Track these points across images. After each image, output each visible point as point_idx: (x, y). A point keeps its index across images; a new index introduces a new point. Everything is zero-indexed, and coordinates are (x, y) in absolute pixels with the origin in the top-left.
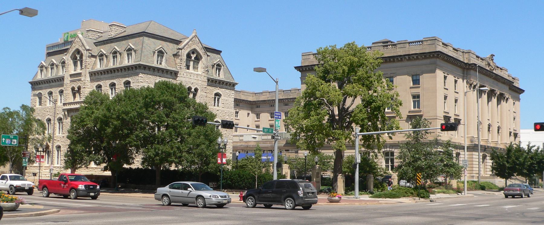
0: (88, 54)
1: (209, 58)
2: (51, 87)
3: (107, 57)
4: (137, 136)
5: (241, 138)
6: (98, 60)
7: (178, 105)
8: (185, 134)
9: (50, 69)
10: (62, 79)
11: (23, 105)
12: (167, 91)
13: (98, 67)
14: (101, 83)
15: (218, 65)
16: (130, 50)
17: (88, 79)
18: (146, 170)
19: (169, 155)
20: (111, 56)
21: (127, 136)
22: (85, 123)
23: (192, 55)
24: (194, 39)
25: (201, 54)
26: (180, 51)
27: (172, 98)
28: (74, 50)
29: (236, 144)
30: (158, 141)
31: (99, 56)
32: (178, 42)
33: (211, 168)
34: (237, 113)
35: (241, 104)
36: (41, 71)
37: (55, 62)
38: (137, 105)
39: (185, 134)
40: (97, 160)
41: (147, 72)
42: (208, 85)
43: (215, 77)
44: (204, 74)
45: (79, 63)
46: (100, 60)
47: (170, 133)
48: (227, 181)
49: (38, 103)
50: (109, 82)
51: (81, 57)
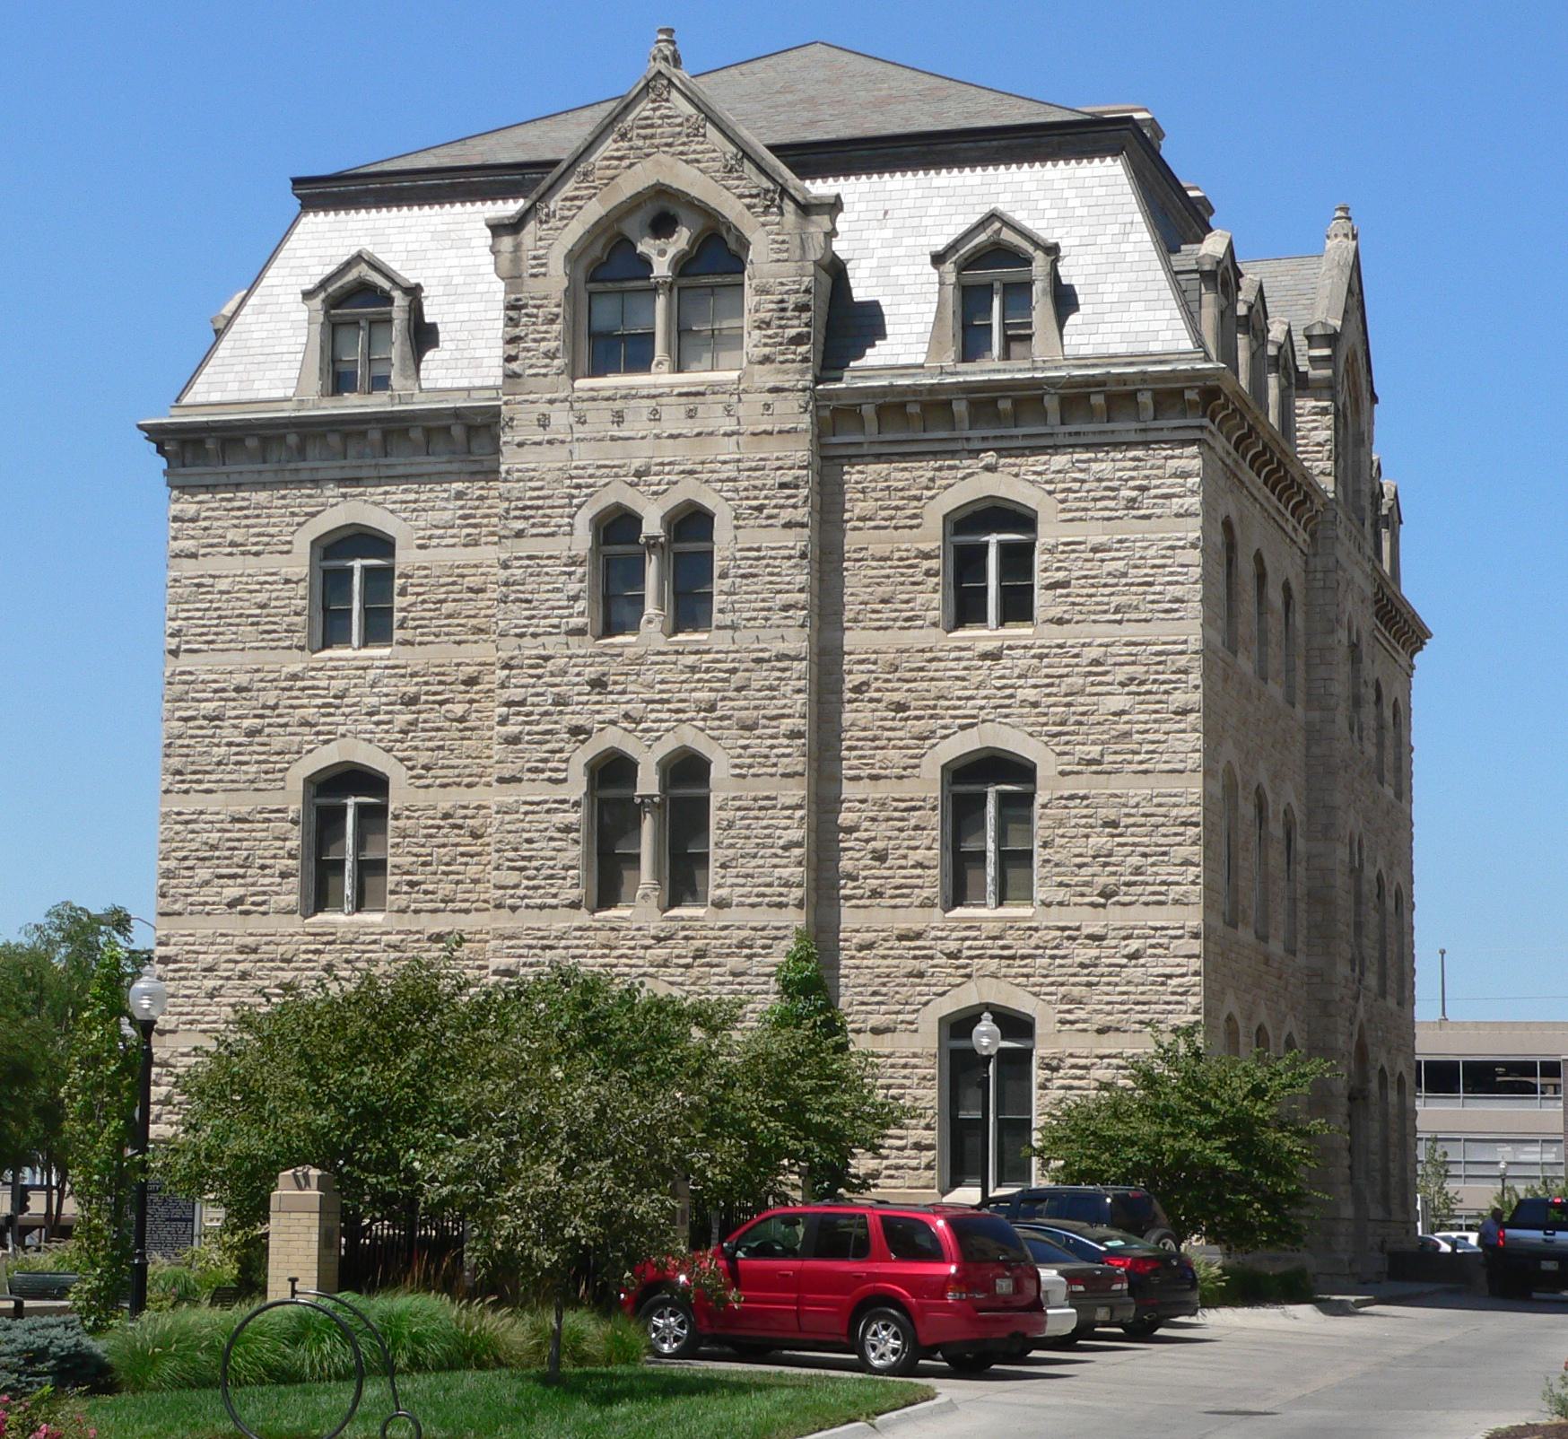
23: (646, 246)
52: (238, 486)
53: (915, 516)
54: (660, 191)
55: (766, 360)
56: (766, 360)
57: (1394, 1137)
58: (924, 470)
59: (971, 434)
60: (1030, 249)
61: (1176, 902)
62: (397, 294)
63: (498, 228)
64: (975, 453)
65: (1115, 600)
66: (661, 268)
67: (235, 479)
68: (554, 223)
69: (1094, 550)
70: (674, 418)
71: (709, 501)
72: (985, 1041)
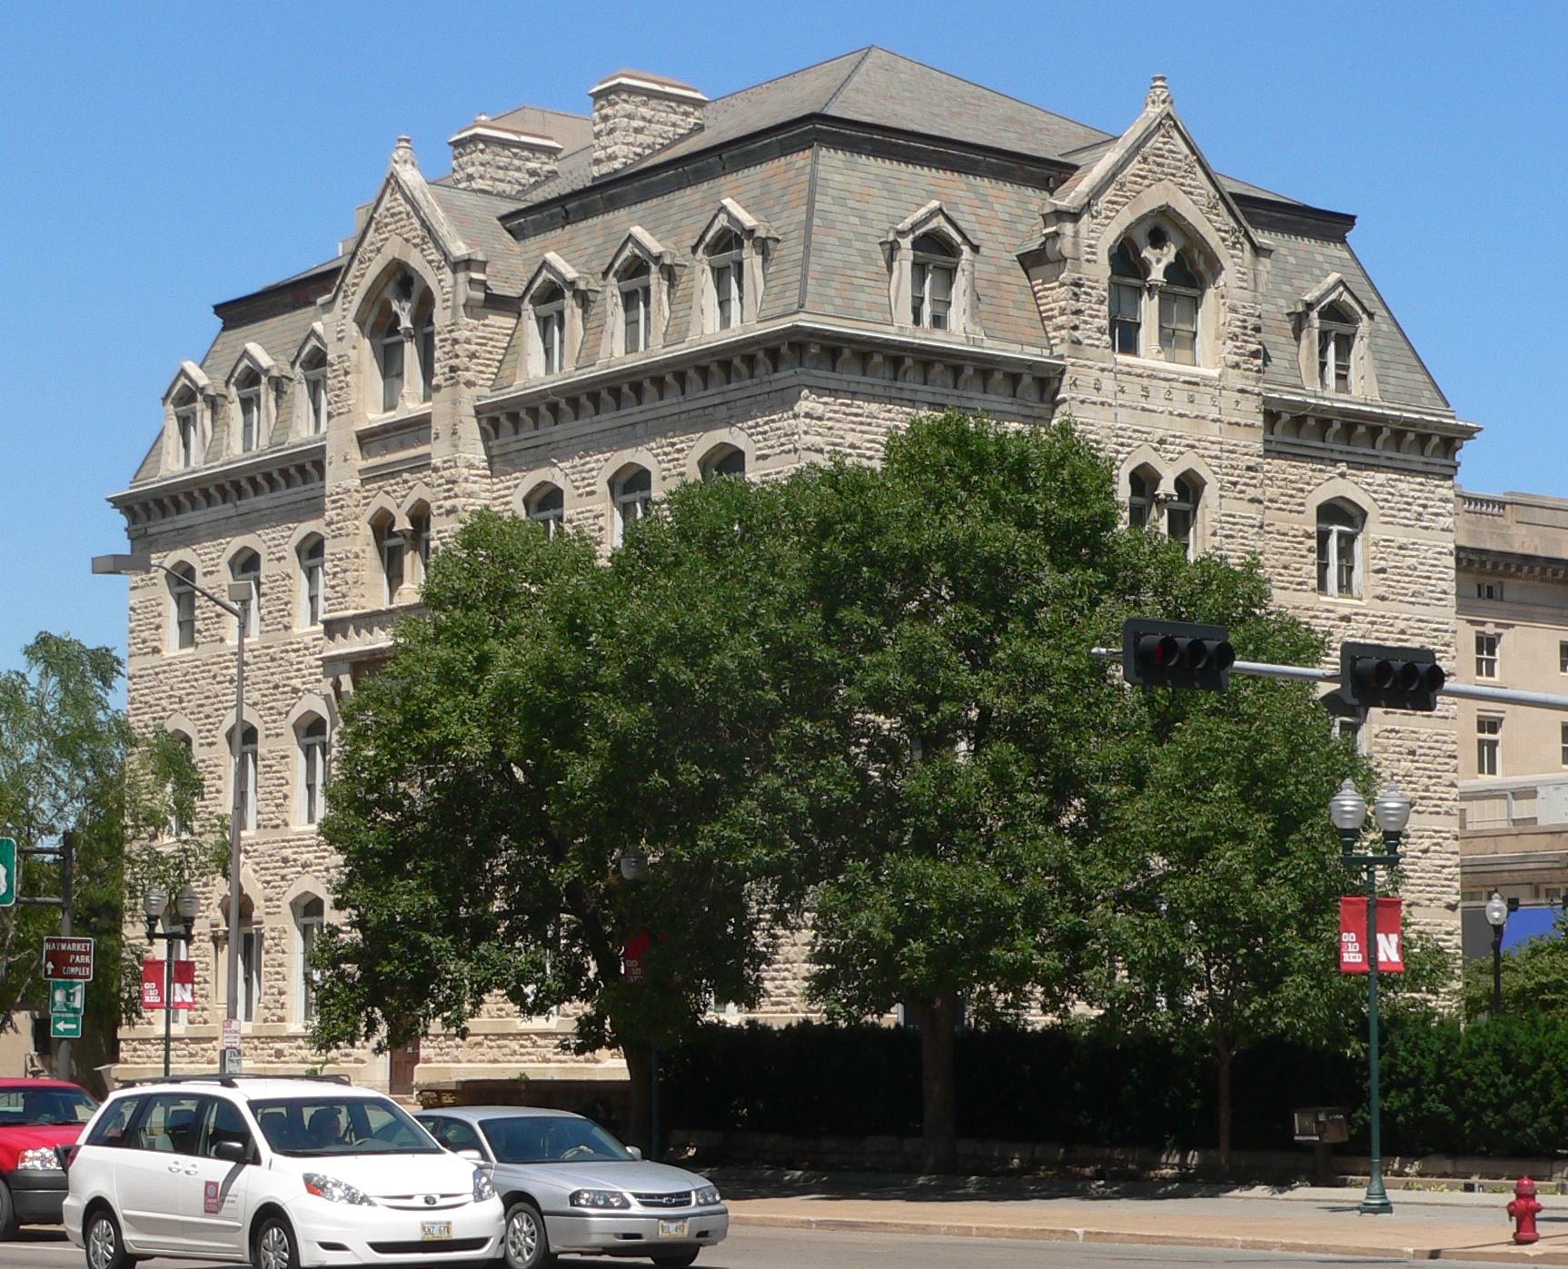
0: (464, 292)
1: (1265, 264)
2: (249, 523)
3: (584, 299)
4: (772, 803)
5: (1522, 809)
6: (531, 326)
7: (1050, 579)
8: (1105, 774)
9: (235, 410)
10: (305, 468)
11: (44, 640)
12: (964, 481)
13: (535, 372)
14: (555, 474)
15: (1335, 313)
16: (728, 241)
17: (475, 452)
18: (828, 1031)
19: (995, 926)
20: (612, 289)
21: (707, 803)
22: (434, 735)
23: (1148, 253)
24: (1157, 141)
25: (1213, 239)
26: (1068, 228)
27: (999, 523)
28: (374, 270)
29: (1484, 852)
30: (920, 833)
31: (536, 301)
32: (1047, 173)
33: (1293, 1007)
34: (1487, 644)
35: (1512, 588)
36: (185, 423)
37: (265, 360)
38: (765, 591)
39: (1105, 774)
40: (523, 978)
41: (853, 378)
42: (1268, 453)
43: (1320, 392)
44: (1236, 379)
45: (410, 352)
46: (544, 324)
47: (1000, 776)
48: (1418, 1100)
49: (172, 632)
50: (605, 465)
51: (423, 315)
52: (854, 395)
53: (1302, 504)
55: (1237, 366)
56: (1237, 366)
58: (1305, 470)
59: (1334, 446)
60: (959, 239)
61: (1447, 813)
62: (965, 248)
64: (1335, 462)
65: (1414, 587)
67: (853, 387)
68: (1100, 220)
69: (1400, 548)
70: (1180, 396)
71: (1204, 473)
72: (1496, 915)
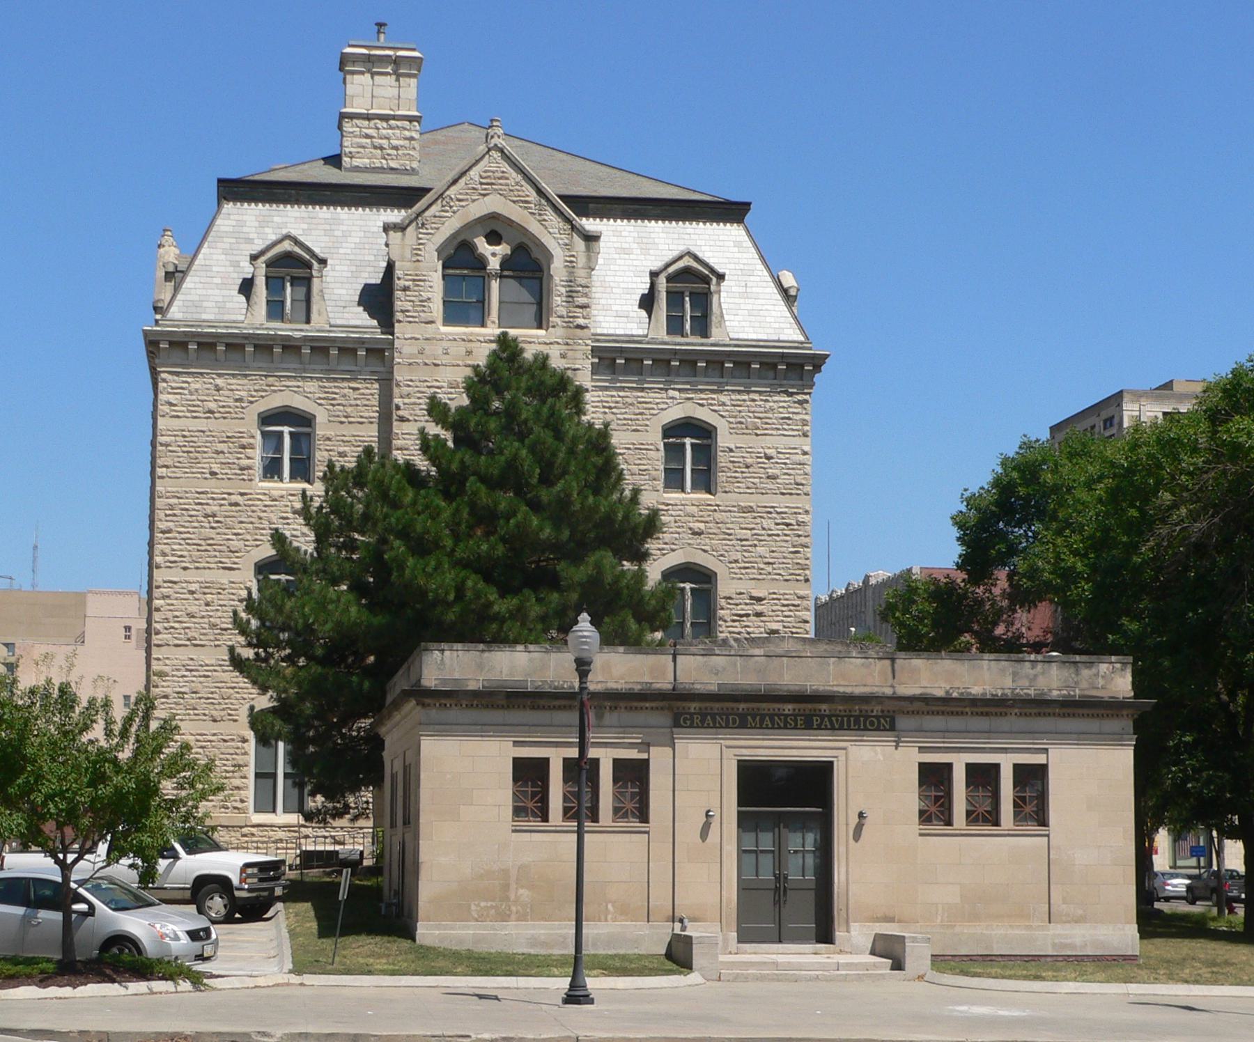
54: (494, 217)
57: (542, 702)
63: (387, 228)
66: (494, 264)
